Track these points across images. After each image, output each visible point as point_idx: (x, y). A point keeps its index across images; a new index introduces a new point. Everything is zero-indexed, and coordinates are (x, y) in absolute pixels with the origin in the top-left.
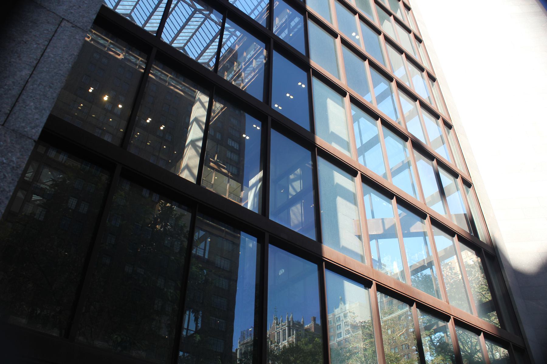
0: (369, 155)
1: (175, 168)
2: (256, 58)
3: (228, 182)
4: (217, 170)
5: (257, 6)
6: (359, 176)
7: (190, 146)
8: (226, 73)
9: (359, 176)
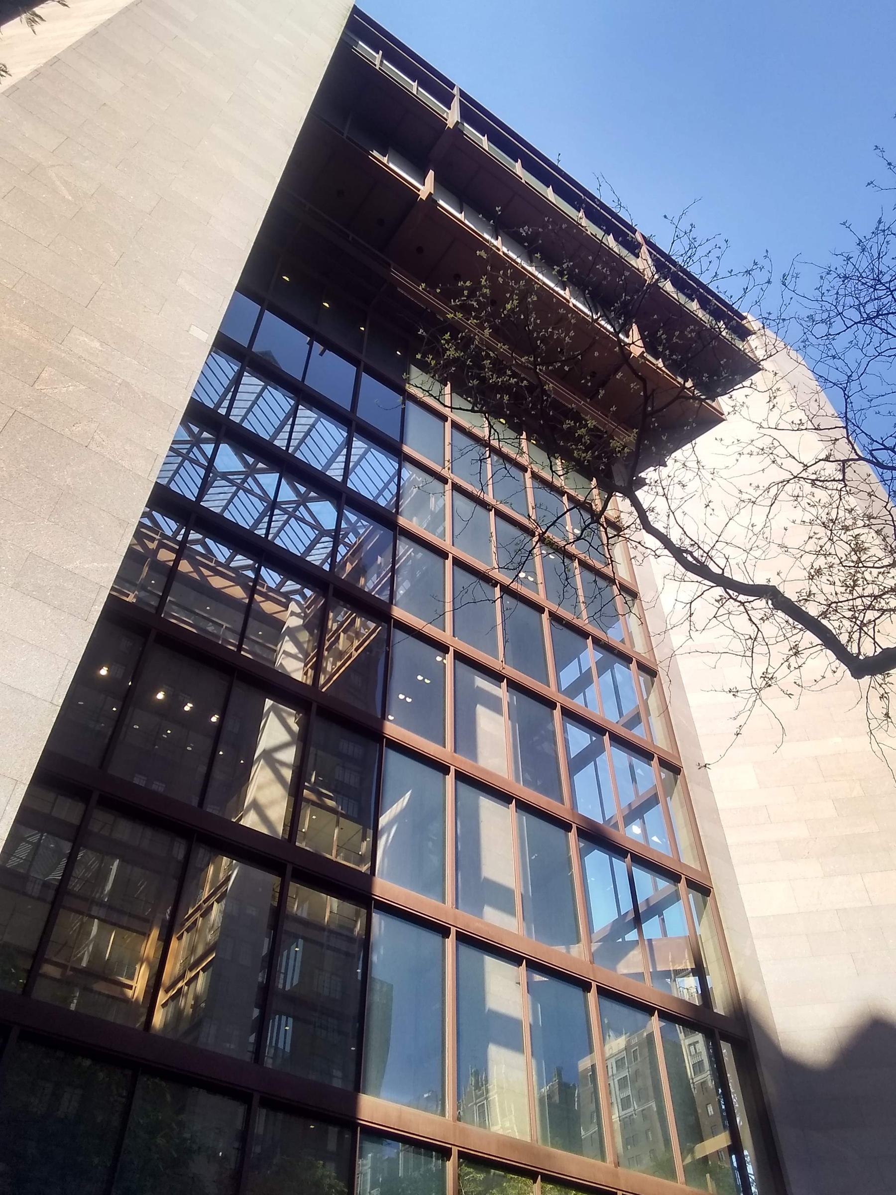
0: (592, 692)
1: (239, 797)
2: (218, 901)
4: (314, 803)
7: (262, 762)
8: (331, 615)
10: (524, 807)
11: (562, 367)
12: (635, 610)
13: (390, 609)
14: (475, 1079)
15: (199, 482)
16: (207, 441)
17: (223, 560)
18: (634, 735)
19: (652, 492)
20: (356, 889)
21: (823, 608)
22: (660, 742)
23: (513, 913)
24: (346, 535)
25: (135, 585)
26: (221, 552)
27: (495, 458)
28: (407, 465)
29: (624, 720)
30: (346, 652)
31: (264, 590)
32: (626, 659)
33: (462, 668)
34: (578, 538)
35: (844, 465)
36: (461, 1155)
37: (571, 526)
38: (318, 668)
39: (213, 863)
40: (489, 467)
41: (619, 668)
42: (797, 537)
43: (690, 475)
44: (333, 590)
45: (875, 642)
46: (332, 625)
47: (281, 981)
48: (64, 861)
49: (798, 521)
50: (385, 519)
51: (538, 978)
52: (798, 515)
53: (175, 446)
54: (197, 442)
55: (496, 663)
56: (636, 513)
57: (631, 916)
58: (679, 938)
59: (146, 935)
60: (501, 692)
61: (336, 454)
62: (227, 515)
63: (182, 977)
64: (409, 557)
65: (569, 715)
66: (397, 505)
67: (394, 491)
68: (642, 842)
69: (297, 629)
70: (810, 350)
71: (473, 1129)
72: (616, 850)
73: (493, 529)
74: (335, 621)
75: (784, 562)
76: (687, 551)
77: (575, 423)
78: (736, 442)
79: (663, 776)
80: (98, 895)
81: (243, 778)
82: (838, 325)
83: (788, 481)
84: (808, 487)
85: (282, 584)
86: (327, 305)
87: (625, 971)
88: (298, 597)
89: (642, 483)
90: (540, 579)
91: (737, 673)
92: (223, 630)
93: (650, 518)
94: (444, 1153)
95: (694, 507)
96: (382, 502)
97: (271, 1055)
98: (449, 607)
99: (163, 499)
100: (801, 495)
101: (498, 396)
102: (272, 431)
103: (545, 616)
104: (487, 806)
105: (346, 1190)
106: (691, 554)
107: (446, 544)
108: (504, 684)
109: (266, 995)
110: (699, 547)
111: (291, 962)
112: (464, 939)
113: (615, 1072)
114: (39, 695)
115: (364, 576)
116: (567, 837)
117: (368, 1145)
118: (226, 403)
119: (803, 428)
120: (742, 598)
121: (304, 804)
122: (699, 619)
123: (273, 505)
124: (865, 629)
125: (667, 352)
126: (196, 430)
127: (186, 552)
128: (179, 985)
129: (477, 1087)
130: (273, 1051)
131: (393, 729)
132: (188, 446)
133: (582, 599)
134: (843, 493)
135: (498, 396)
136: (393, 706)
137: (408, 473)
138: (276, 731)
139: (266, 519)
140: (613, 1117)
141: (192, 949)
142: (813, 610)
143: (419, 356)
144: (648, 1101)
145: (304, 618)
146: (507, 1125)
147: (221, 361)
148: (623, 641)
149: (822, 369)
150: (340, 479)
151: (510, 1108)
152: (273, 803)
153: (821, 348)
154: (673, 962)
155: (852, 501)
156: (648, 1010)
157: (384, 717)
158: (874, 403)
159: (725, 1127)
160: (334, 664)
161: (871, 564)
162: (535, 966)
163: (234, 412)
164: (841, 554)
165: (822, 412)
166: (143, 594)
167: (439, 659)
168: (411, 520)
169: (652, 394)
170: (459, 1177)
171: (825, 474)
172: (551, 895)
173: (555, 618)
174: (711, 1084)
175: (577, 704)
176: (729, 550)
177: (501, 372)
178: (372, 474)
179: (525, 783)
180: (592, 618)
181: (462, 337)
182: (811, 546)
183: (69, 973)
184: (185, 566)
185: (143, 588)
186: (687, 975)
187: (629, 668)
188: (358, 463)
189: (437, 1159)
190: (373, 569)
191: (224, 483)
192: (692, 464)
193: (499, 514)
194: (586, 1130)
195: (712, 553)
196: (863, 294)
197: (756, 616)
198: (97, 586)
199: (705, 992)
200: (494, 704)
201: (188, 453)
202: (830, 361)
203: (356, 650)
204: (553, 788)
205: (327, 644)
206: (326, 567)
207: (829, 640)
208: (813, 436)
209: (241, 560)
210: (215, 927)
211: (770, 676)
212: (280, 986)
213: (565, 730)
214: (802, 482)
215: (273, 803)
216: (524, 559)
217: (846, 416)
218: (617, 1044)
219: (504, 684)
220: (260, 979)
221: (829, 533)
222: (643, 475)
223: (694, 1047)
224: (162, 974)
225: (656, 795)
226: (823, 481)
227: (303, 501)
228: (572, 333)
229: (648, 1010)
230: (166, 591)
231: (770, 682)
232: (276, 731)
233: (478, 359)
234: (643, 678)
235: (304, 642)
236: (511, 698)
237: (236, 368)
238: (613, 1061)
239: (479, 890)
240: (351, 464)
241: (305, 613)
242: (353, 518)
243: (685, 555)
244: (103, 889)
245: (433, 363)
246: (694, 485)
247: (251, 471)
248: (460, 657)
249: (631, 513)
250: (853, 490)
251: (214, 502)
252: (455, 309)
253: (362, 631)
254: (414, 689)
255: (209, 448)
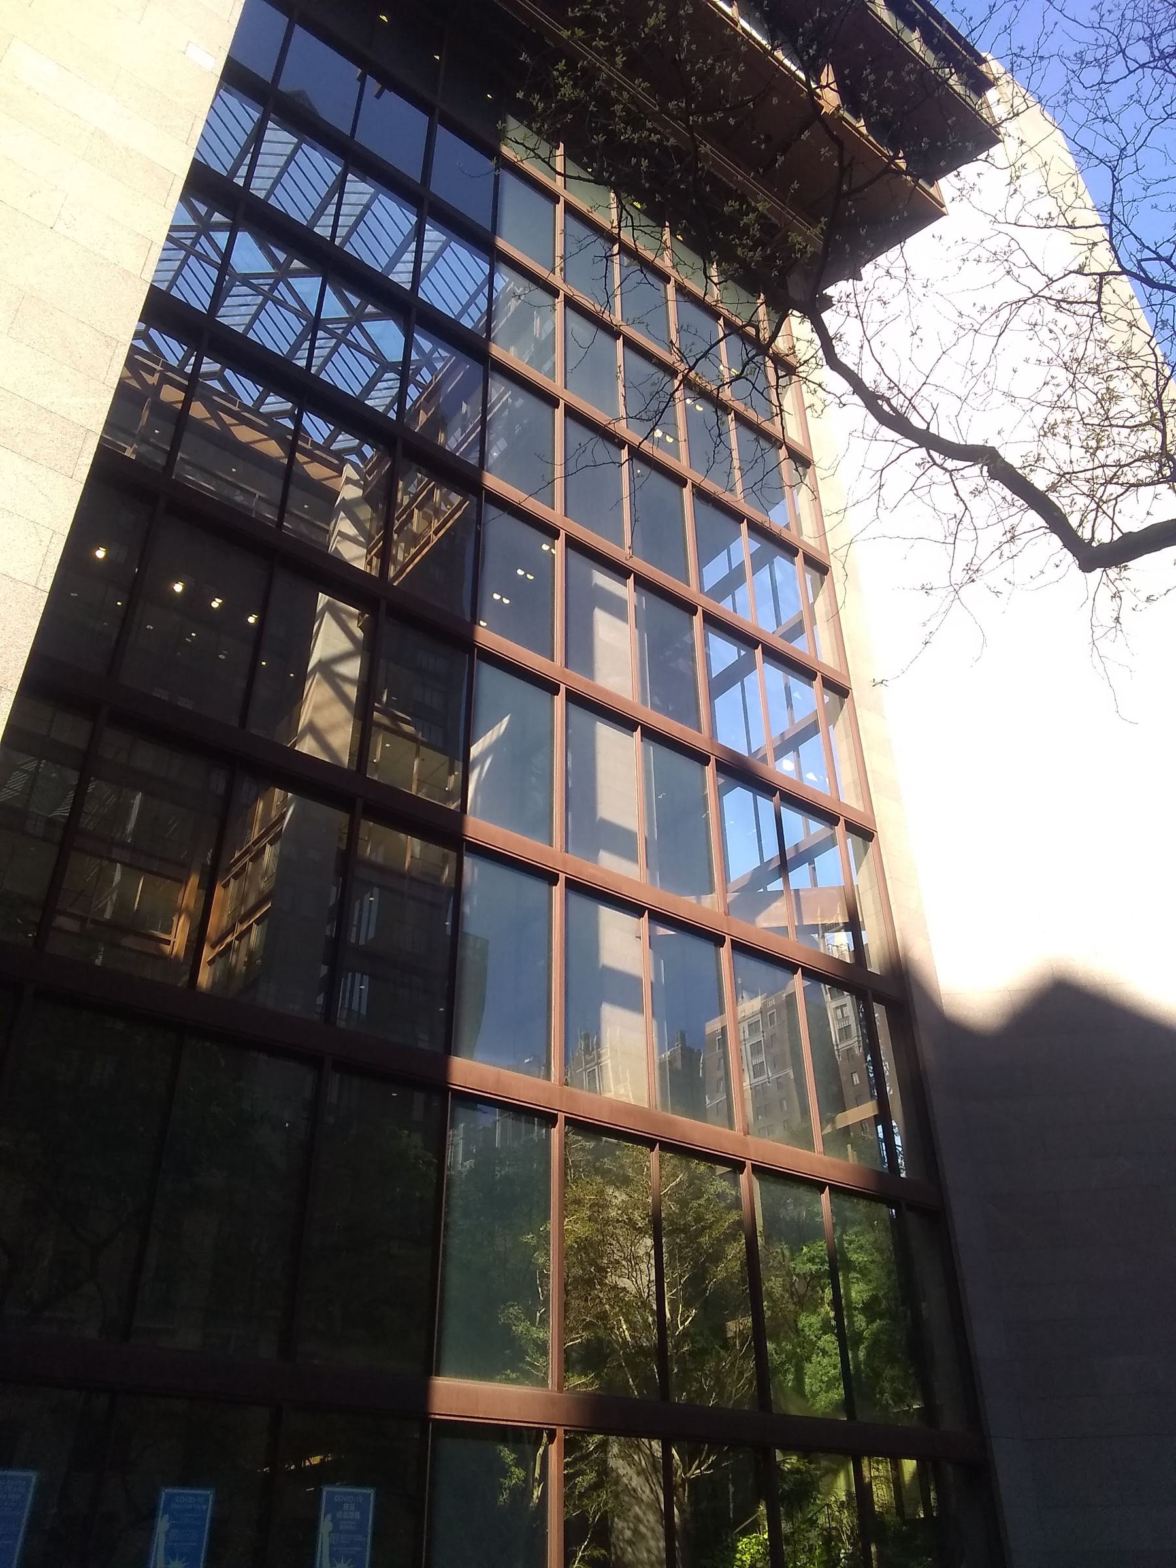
0: (743, 594)
2: (271, 843)
3: (418, 754)
5: (468, 305)
6: (842, 822)
9: (842, 822)
10: (651, 735)
11: (726, 118)
12: (807, 481)
13: (480, 476)
14: (585, 1042)
15: (211, 288)
16: (219, 227)
17: (250, 403)
18: (795, 649)
19: (842, 312)
20: (445, 829)
21: (1053, 478)
22: (826, 658)
23: (634, 858)
24: (418, 371)
25: (133, 435)
26: (246, 390)
27: (626, 261)
28: (503, 268)
29: (782, 630)
30: (421, 536)
31: (309, 447)
32: (790, 550)
33: (577, 559)
34: (738, 378)
35: (1101, 282)
36: (568, 1121)
37: (726, 360)
38: (385, 556)
39: (262, 798)
40: (617, 267)
41: (780, 562)
42: (1029, 381)
43: (896, 285)
44: (404, 448)
45: (1114, 523)
46: (403, 499)
47: (354, 935)
48: (72, 794)
49: (1033, 361)
50: (471, 346)
51: (662, 931)
52: (1034, 350)
53: (175, 235)
54: (204, 228)
55: (622, 553)
56: (818, 342)
57: (777, 863)
58: (832, 888)
59: (183, 882)
60: (626, 591)
61: (401, 250)
62: (251, 335)
63: (231, 930)
64: (505, 405)
65: (714, 622)
66: (488, 328)
67: (484, 308)
68: (794, 777)
69: (355, 502)
70: (1072, 105)
71: (582, 1094)
72: (762, 786)
73: (620, 362)
74: (405, 492)
75: (1011, 414)
76: (882, 397)
77: (741, 205)
78: (960, 241)
79: (827, 699)
80: (118, 836)
81: (295, 696)
82: (1118, 67)
83: (1025, 302)
84: (1050, 311)
85: (332, 438)
86: (384, 18)
87: (765, 925)
88: (354, 458)
89: (827, 303)
90: (682, 434)
91: (934, 564)
92: (256, 499)
93: (837, 350)
94: (549, 1119)
95: (896, 337)
96: (467, 322)
97: (344, 1017)
98: (559, 471)
99: (161, 310)
100: (1040, 322)
101: (634, 160)
102: (309, 213)
103: (687, 492)
104: (606, 734)
105: (435, 1161)
106: (888, 401)
107: (555, 386)
108: (631, 582)
109: (337, 952)
110: (900, 391)
111: (365, 915)
112: (575, 886)
113: (747, 1036)
114: (18, 577)
115: (444, 430)
116: (704, 771)
117: (461, 1112)
118: (243, 171)
119: (1053, 224)
120: (951, 464)
121: (374, 729)
122: (890, 494)
123: (315, 324)
124: (1105, 507)
125: (875, 103)
126: (203, 209)
127: (198, 390)
128: (229, 939)
129: (587, 1051)
130: (345, 1012)
131: (486, 636)
132: (192, 235)
133: (736, 463)
134: (1095, 320)
135: (634, 160)
136: (486, 608)
137: (504, 280)
138: (332, 638)
139: (306, 345)
140: (743, 1084)
141: (242, 898)
142: (1040, 480)
143: (520, 95)
144: (784, 1067)
145: (364, 488)
146: (622, 1091)
147: (233, 102)
148: (787, 526)
149: (1086, 138)
150: (408, 287)
151: (626, 1068)
152: (334, 727)
153: (1089, 104)
154: (822, 916)
155: (1104, 332)
156: (790, 967)
157: (475, 621)
158: (1150, 192)
159: (872, 1096)
160: (406, 551)
161: (1121, 423)
162: (659, 917)
163: (255, 183)
164: (1083, 408)
165: (1079, 203)
166: (144, 448)
167: (545, 547)
168: (508, 350)
169: (850, 165)
170: (565, 1145)
171: (1072, 295)
172: (681, 837)
173: (701, 494)
174: (858, 1052)
175: (724, 608)
176: (936, 397)
177: (637, 126)
178: (452, 280)
179: (654, 706)
180: (749, 490)
181: (583, 69)
182: (1047, 395)
183: (89, 926)
184: (198, 410)
185: (144, 440)
186: (839, 931)
187: (793, 563)
188: (432, 264)
189: (540, 1125)
190: (456, 421)
191: (245, 290)
192: (898, 272)
193: (630, 344)
194: (711, 1099)
195: (916, 402)
196: (1159, 18)
197: (964, 487)
198: (82, 430)
199: (859, 949)
200: (617, 608)
201: (194, 244)
202: (1099, 126)
203: (436, 533)
204: (689, 714)
205: (397, 524)
206: (392, 415)
207: (1056, 522)
208: (1064, 237)
209: (275, 403)
210: (270, 873)
211: (975, 568)
212: (353, 941)
213: (706, 643)
214: (1044, 302)
215: (334, 727)
216: (663, 405)
217: (1111, 210)
218: (751, 1006)
219: (631, 582)
220: (328, 933)
221: (1071, 377)
222: (829, 291)
223: (840, 1010)
224: (205, 930)
225: (816, 723)
226: (1071, 303)
227: (356, 318)
228: (741, 67)
229: (790, 967)
230: (176, 444)
231: (974, 577)
232: (332, 638)
233: (605, 102)
234: (810, 576)
235: (366, 521)
236: (639, 601)
237: (256, 116)
238: (745, 1025)
239: (593, 832)
240: (423, 265)
241: (365, 480)
242: (426, 345)
243: (880, 402)
244: (124, 828)
245: (541, 106)
246: (898, 304)
247: (283, 274)
248: (573, 544)
249: (811, 342)
250: (1109, 318)
251: (235, 314)
252: (570, 24)
253: (443, 508)
254: (511, 587)
255: (222, 238)
